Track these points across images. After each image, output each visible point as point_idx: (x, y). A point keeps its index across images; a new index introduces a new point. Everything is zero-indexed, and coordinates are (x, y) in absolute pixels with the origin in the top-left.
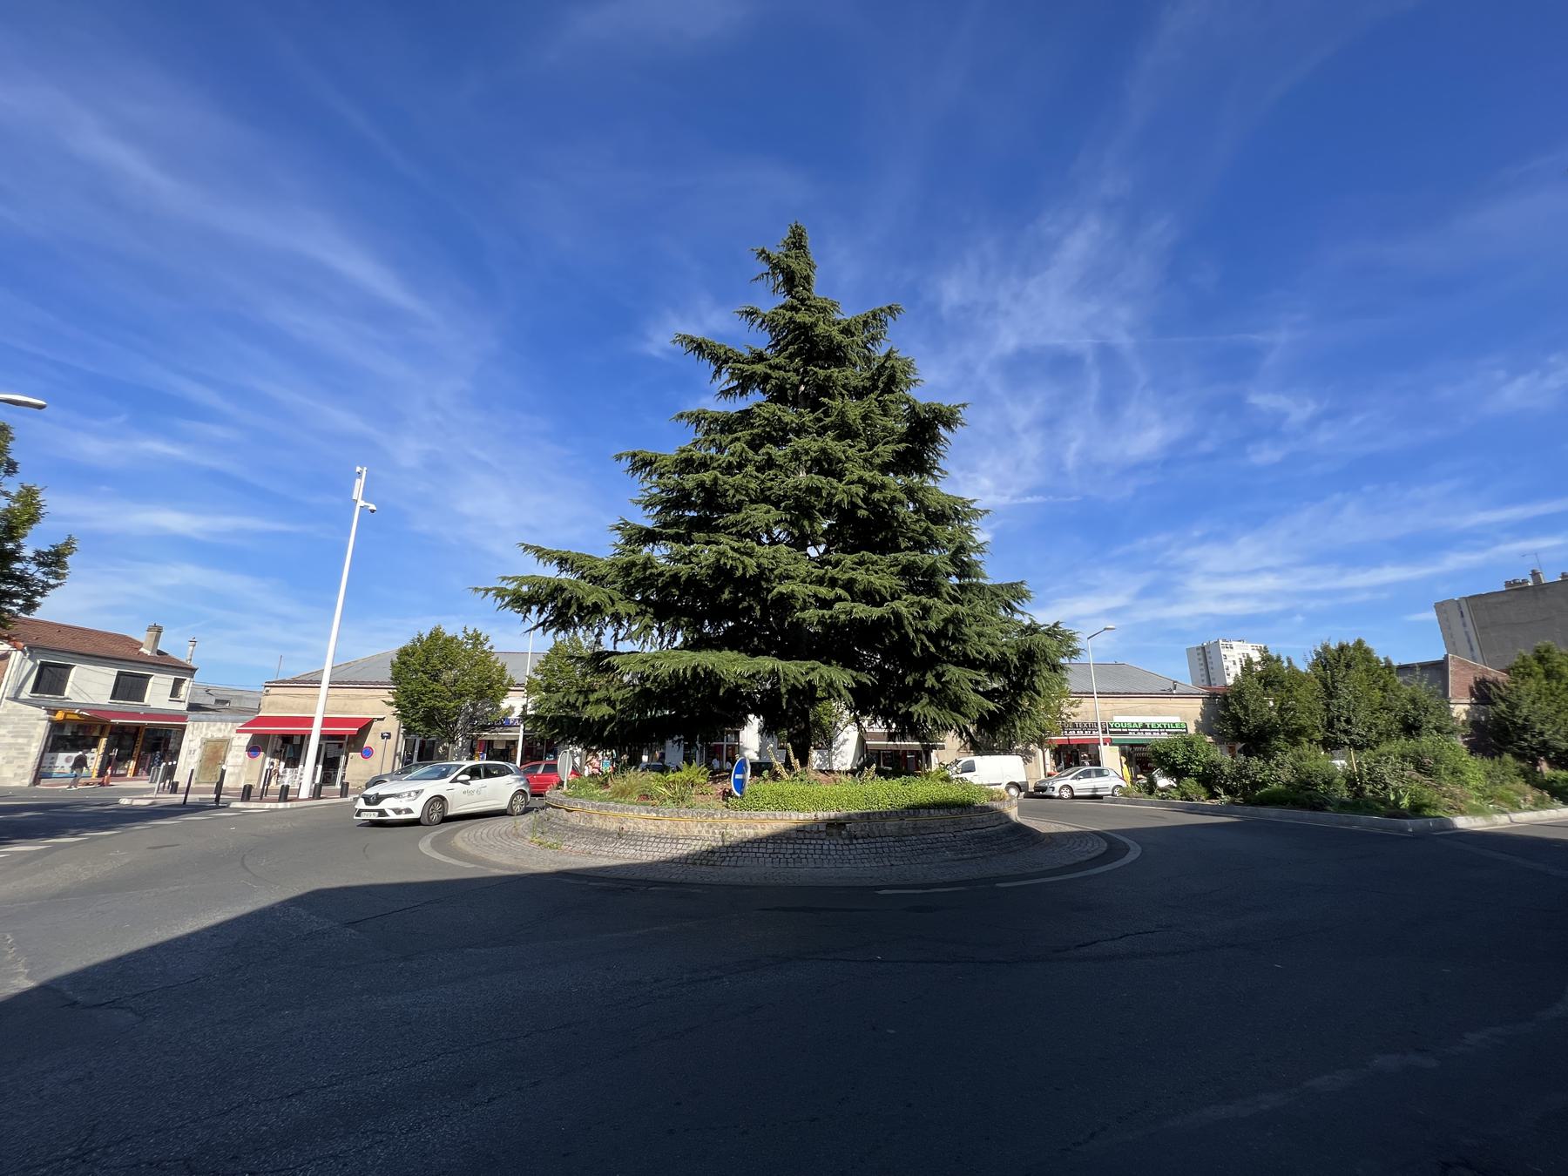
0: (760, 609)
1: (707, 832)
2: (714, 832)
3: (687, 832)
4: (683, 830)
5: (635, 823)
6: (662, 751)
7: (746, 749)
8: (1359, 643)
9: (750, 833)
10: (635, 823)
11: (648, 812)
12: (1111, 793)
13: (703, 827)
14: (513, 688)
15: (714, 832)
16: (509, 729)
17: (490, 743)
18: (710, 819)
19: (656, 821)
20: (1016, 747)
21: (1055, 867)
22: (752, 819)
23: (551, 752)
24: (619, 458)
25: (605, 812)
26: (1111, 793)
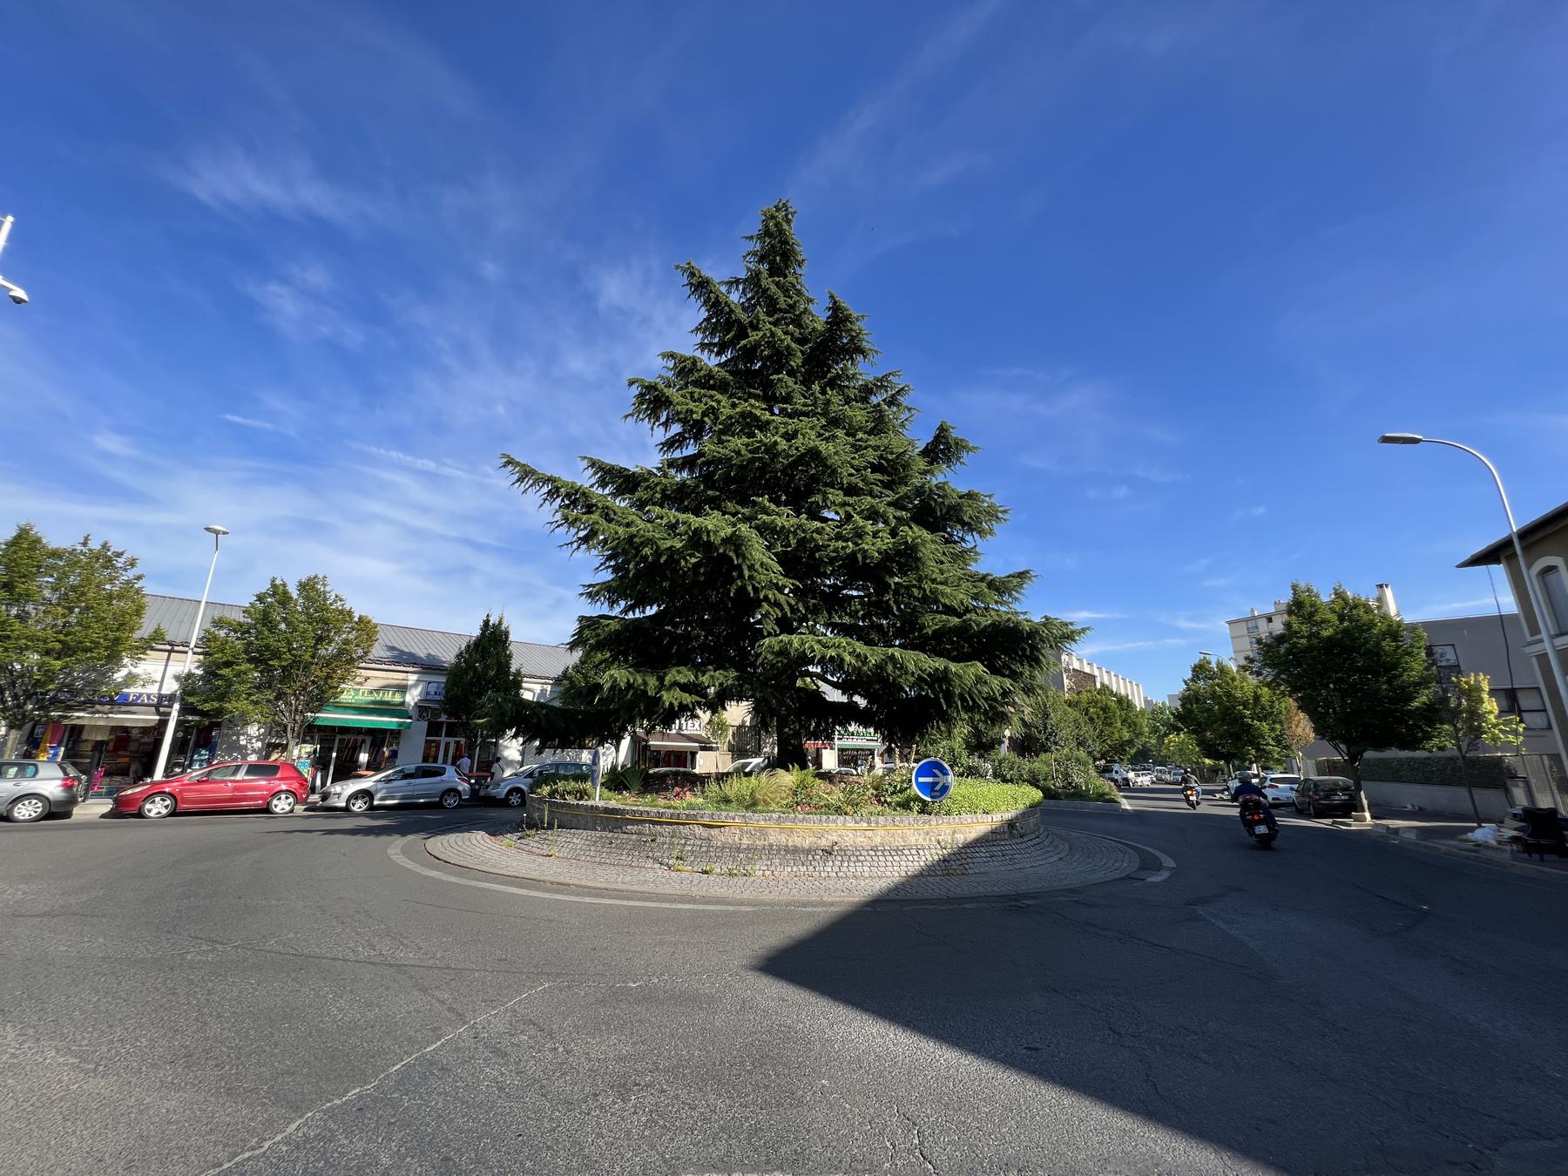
0: (750, 594)
1: (925, 840)
2: (930, 839)
3: (904, 841)
4: (900, 840)
5: (840, 836)
6: (394, 747)
7: (519, 750)
8: (307, 587)
9: (961, 839)
10: (840, 836)
11: (856, 822)
12: (344, 804)
13: (920, 835)
14: (363, 665)
15: (930, 839)
16: (124, 708)
17: (76, 731)
18: (927, 826)
19: (867, 832)
20: (765, 750)
21: (599, 885)
22: (962, 823)
23: (204, 747)
24: (631, 383)
25: (789, 825)
26: (344, 804)
